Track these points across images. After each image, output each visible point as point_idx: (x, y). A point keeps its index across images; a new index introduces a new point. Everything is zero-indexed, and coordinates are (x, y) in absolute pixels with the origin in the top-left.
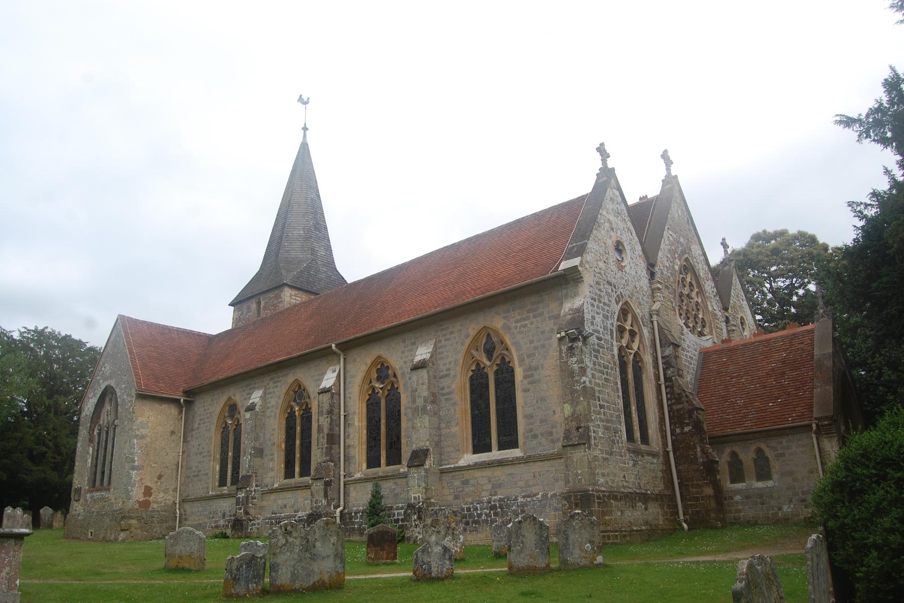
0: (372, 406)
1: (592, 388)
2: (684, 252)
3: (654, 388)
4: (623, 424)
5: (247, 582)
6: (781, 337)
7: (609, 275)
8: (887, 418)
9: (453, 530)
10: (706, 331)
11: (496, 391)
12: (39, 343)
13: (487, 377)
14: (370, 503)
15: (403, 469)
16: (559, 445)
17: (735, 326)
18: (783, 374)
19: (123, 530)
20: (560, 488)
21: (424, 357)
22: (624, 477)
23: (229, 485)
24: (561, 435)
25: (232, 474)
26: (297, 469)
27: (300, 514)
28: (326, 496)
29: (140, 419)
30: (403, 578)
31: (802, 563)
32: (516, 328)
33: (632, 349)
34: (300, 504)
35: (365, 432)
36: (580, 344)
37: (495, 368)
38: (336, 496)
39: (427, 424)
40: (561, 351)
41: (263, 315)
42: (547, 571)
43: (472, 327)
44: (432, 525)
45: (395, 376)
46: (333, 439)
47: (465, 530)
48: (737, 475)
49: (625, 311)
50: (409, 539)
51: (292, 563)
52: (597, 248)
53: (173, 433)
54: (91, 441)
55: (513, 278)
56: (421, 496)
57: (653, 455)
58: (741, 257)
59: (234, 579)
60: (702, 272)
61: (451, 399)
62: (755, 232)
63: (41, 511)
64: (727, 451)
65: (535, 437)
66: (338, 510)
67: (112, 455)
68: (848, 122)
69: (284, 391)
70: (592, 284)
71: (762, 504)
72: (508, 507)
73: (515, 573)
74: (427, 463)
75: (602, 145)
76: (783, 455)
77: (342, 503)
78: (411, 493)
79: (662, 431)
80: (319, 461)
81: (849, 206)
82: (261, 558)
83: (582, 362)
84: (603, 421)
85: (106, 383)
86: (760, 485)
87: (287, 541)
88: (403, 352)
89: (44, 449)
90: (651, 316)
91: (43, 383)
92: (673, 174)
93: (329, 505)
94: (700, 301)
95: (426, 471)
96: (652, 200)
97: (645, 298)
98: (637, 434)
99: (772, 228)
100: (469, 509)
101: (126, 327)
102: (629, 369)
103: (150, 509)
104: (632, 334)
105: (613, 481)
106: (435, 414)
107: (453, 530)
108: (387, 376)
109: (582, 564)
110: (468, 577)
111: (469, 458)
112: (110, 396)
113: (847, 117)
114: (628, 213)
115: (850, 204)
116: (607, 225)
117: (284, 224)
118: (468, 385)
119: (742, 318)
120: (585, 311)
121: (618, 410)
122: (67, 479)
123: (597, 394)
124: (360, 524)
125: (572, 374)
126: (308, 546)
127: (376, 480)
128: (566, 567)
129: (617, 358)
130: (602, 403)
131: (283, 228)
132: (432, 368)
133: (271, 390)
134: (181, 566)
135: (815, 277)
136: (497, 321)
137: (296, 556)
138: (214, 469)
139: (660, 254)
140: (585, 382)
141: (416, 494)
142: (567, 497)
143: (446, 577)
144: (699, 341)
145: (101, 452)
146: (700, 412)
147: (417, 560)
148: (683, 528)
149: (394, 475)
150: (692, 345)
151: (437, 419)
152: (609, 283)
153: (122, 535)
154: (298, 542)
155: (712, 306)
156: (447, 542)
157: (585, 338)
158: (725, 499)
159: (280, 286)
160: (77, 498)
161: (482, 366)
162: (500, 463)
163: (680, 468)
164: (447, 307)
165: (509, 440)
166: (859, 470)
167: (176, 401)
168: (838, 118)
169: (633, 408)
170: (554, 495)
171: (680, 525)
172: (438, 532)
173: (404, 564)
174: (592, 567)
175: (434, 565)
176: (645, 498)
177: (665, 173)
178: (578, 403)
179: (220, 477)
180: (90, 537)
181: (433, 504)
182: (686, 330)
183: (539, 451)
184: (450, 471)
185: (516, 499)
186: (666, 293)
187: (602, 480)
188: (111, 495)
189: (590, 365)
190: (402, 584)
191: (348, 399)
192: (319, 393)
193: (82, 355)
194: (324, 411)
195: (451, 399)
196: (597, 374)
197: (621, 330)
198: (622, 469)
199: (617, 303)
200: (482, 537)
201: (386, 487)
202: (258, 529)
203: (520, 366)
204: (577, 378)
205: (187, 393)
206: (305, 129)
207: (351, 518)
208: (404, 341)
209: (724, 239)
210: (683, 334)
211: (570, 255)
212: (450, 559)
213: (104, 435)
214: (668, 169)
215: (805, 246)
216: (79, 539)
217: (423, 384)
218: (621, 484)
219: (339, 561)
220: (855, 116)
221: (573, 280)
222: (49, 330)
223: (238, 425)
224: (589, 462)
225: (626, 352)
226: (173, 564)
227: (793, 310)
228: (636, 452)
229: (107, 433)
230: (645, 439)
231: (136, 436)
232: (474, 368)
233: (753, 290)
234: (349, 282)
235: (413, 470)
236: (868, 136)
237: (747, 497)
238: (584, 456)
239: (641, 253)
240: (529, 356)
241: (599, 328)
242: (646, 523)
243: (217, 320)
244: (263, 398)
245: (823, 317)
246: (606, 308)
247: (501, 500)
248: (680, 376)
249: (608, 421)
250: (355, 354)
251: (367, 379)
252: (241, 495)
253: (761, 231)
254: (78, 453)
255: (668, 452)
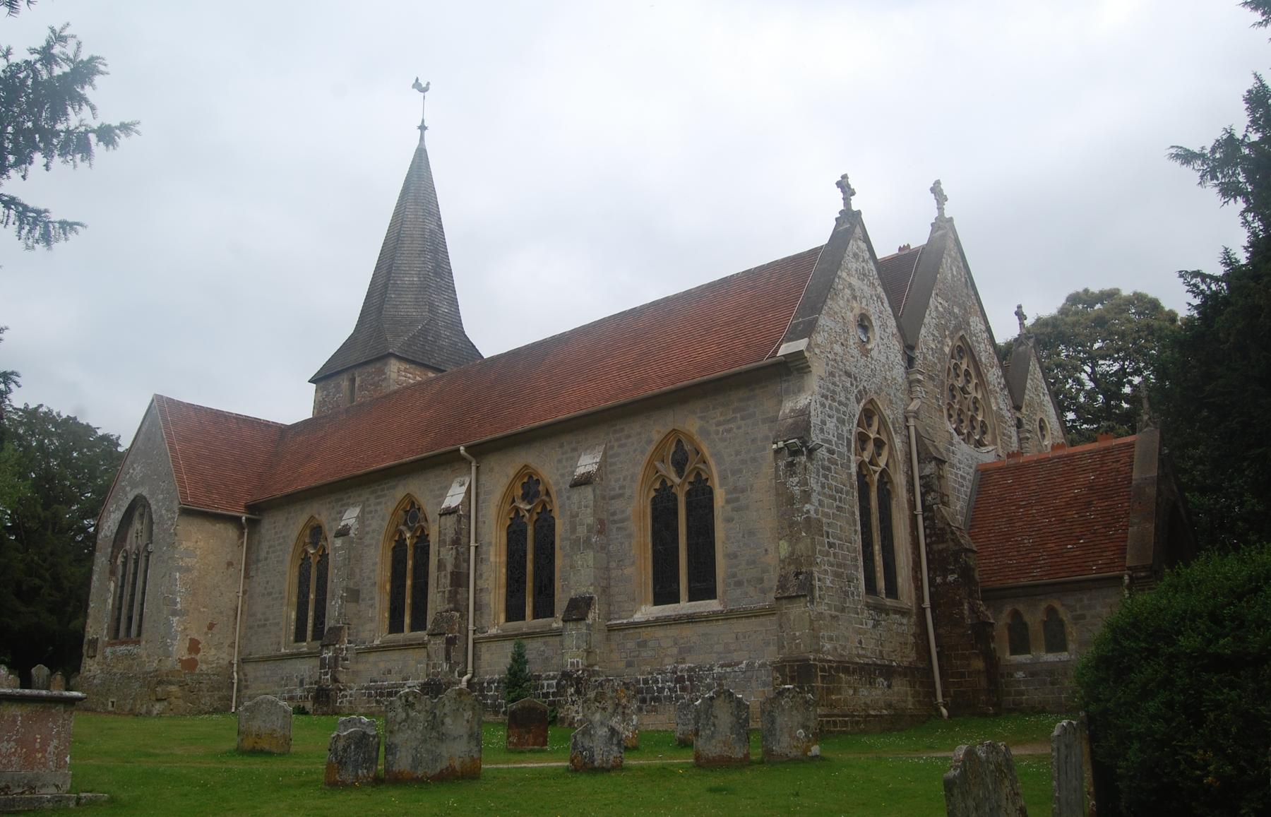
0: (515, 535)
1: (819, 520)
2: (958, 328)
3: (908, 522)
4: (861, 570)
5: (356, 768)
6: (1090, 452)
7: (851, 357)
8: (1167, 579)
9: (624, 707)
10: (987, 439)
11: (688, 520)
12: (30, 427)
13: (676, 499)
14: (509, 670)
15: (557, 624)
16: (772, 596)
17: (1030, 432)
18: (1090, 503)
19: (158, 700)
20: (771, 655)
21: (589, 468)
22: (860, 642)
23: (309, 639)
24: (775, 583)
25: (313, 624)
26: (407, 620)
27: (410, 683)
28: (448, 658)
29: (185, 545)
30: (556, 768)
31: (1045, 758)
32: (717, 433)
33: (877, 465)
34: (410, 670)
35: (504, 570)
36: (804, 459)
37: (687, 487)
38: (462, 659)
39: (591, 563)
40: (777, 468)
41: (358, 399)
42: (746, 762)
43: (655, 430)
44: (596, 700)
45: (548, 493)
46: (459, 580)
47: (640, 709)
48: (1020, 644)
49: (869, 414)
50: (562, 720)
51: (414, 744)
52: (832, 325)
53: (230, 564)
54: (113, 573)
55: (713, 361)
56: (581, 661)
57: (903, 613)
58: (1049, 329)
59: (340, 762)
60: (985, 354)
61: (625, 529)
62: (1072, 290)
63: (33, 671)
64: (1008, 609)
65: (739, 584)
66: (465, 678)
67: (144, 593)
68: (1186, 157)
69: (391, 510)
70: (823, 375)
71: (1053, 684)
72: (700, 679)
73: (704, 764)
74: (591, 616)
75: (845, 177)
76: (1083, 617)
77: (470, 668)
78: (566, 657)
79: (917, 580)
80: (439, 609)
81: (1181, 276)
82: (374, 737)
83: (806, 484)
84: (832, 565)
85: (136, 492)
86: (1051, 657)
87: (408, 715)
88: (560, 461)
89: (37, 581)
90: (907, 419)
91: (36, 486)
92: (947, 215)
93: (452, 670)
94: (979, 397)
95: (588, 626)
96: (916, 251)
97: (899, 394)
98: (881, 584)
99: (1096, 286)
100: (646, 682)
101: (166, 414)
102: (873, 493)
103: (197, 671)
104: (879, 444)
105: (844, 648)
106: (603, 548)
107: (624, 707)
108: (537, 494)
109: (791, 755)
110: (642, 768)
111: (648, 611)
112: (141, 510)
113: (1186, 150)
114: (879, 273)
115: (1182, 274)
116: (847, 292)
117: (391, 266)
118: (649, 510)
119: (1041, 420)
120: (813, 413)
121: (855, 550)
122: (75, 624)
123: (825, 528)
124: (495, 698)
125: (791, 500)
126: (435, 723)
127: (519, 637)
128: (771, 759)
129: (855, 478)
130: (831, 540)
131: (389, 273)
132: (602, 482)
133: (372, 508)
134: (258, 747)
135: (1150, 361)
136: (691, 422)
137: (419, 736)
138: (288, 617)
139: (923, 331)
140: (808, 511)
141: (573, 658)
142: (779, 667)
143: (613, 768)
144: (976, 454)
145: (128, 589)
146: (970, 554)
147: (575, 744)
148: (941, 715)
149: (542, 632)
150: (965, 460)
151: (605, 555)
152: (848, 374)
153: (158, 707)
154: (422, 717)
155: (998, 404)
156: (615, 722)
157: (811, 451)
158: (1002, 676)
159: (385, 357)
160: (91, 653)
161: (669, 484)
162: (691, 619)
163: (941, 631)
164: (622, 400)
165: (703, 587)
166: (1126, 643)
167: (235, 520)
168: (1174, 151)
169: (877, 548)
170: (763, 665)
171: (938, 710)
172: (604, 709)
173: (557, 751)
174: (805, 760)
175: (597, 752)
176: (888, 672)
177: (936, 214)
178: (798, 540)
179: (297, 628)
180: (110, 708)
181: (596, 673)
182: (956, 438)
183: (744, 604)
184: (621, 628)
185: (711, 669)
186: (930, 386)
187: (828, 646)
188: (141, 651)
189: (817, 488)
190: (556, 775)
191: (480, 524)
192: (441, 515)
193: (91, 446)
194: (448, 540)
195: (625, 529)
196: (826, 501)
197: (863, 439)
198: (858, 632)
199: (858, 402)
200: (663, 720)
201: (533, 648)
202: (350, 702)
203: (721, 485)
204: (797, 506)
205: (250, 508)
206: (423, 128)
207: (482, 690)
208: (562, 446)
209: (1019, 307)
210: (952, 445)
211: (794, 336)
212: (619, 744)
213: (131, 565)
214: (940, 209)
215: (1143, 313)
216: (94, 711)
217: (586, 507)
218: (854, 652)
219: (473, 743)
220: (1197, 150)
221: (798, 370)
222: (44, 409)
223: (324, 557)
224: (811, 622)
225: (868, 470)
226: (248, 744)
227: (1125, 405)
228: (879, 609)
229: (136, 562)
230: (892, 590)
231: (179, 569)
232: (657, 486)
233: (1064, 377)
234: (486, 355)
235: (571, 625)
236: (1214, 177)
237: (1033, 675)
238: (804, 613)
239: (895, 330)
240: (734, 473)
241: (831, 437)
242: (889, 706)
243: (288, 401)
244: (360, 519)
245: (1147, 425)
246: (842, 409)
247: (690, 670)
248: (944, 504)
249: (839, 566)
250: (492, 461)
251: (509, 497)
252: (328, 654)
253: (1080, 290)
254: (93, 590)
255: (924, 609)
